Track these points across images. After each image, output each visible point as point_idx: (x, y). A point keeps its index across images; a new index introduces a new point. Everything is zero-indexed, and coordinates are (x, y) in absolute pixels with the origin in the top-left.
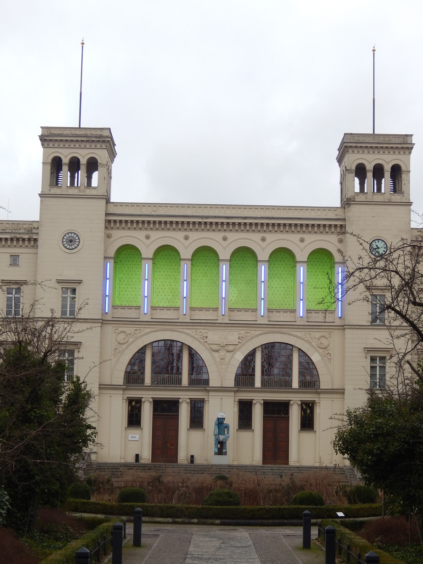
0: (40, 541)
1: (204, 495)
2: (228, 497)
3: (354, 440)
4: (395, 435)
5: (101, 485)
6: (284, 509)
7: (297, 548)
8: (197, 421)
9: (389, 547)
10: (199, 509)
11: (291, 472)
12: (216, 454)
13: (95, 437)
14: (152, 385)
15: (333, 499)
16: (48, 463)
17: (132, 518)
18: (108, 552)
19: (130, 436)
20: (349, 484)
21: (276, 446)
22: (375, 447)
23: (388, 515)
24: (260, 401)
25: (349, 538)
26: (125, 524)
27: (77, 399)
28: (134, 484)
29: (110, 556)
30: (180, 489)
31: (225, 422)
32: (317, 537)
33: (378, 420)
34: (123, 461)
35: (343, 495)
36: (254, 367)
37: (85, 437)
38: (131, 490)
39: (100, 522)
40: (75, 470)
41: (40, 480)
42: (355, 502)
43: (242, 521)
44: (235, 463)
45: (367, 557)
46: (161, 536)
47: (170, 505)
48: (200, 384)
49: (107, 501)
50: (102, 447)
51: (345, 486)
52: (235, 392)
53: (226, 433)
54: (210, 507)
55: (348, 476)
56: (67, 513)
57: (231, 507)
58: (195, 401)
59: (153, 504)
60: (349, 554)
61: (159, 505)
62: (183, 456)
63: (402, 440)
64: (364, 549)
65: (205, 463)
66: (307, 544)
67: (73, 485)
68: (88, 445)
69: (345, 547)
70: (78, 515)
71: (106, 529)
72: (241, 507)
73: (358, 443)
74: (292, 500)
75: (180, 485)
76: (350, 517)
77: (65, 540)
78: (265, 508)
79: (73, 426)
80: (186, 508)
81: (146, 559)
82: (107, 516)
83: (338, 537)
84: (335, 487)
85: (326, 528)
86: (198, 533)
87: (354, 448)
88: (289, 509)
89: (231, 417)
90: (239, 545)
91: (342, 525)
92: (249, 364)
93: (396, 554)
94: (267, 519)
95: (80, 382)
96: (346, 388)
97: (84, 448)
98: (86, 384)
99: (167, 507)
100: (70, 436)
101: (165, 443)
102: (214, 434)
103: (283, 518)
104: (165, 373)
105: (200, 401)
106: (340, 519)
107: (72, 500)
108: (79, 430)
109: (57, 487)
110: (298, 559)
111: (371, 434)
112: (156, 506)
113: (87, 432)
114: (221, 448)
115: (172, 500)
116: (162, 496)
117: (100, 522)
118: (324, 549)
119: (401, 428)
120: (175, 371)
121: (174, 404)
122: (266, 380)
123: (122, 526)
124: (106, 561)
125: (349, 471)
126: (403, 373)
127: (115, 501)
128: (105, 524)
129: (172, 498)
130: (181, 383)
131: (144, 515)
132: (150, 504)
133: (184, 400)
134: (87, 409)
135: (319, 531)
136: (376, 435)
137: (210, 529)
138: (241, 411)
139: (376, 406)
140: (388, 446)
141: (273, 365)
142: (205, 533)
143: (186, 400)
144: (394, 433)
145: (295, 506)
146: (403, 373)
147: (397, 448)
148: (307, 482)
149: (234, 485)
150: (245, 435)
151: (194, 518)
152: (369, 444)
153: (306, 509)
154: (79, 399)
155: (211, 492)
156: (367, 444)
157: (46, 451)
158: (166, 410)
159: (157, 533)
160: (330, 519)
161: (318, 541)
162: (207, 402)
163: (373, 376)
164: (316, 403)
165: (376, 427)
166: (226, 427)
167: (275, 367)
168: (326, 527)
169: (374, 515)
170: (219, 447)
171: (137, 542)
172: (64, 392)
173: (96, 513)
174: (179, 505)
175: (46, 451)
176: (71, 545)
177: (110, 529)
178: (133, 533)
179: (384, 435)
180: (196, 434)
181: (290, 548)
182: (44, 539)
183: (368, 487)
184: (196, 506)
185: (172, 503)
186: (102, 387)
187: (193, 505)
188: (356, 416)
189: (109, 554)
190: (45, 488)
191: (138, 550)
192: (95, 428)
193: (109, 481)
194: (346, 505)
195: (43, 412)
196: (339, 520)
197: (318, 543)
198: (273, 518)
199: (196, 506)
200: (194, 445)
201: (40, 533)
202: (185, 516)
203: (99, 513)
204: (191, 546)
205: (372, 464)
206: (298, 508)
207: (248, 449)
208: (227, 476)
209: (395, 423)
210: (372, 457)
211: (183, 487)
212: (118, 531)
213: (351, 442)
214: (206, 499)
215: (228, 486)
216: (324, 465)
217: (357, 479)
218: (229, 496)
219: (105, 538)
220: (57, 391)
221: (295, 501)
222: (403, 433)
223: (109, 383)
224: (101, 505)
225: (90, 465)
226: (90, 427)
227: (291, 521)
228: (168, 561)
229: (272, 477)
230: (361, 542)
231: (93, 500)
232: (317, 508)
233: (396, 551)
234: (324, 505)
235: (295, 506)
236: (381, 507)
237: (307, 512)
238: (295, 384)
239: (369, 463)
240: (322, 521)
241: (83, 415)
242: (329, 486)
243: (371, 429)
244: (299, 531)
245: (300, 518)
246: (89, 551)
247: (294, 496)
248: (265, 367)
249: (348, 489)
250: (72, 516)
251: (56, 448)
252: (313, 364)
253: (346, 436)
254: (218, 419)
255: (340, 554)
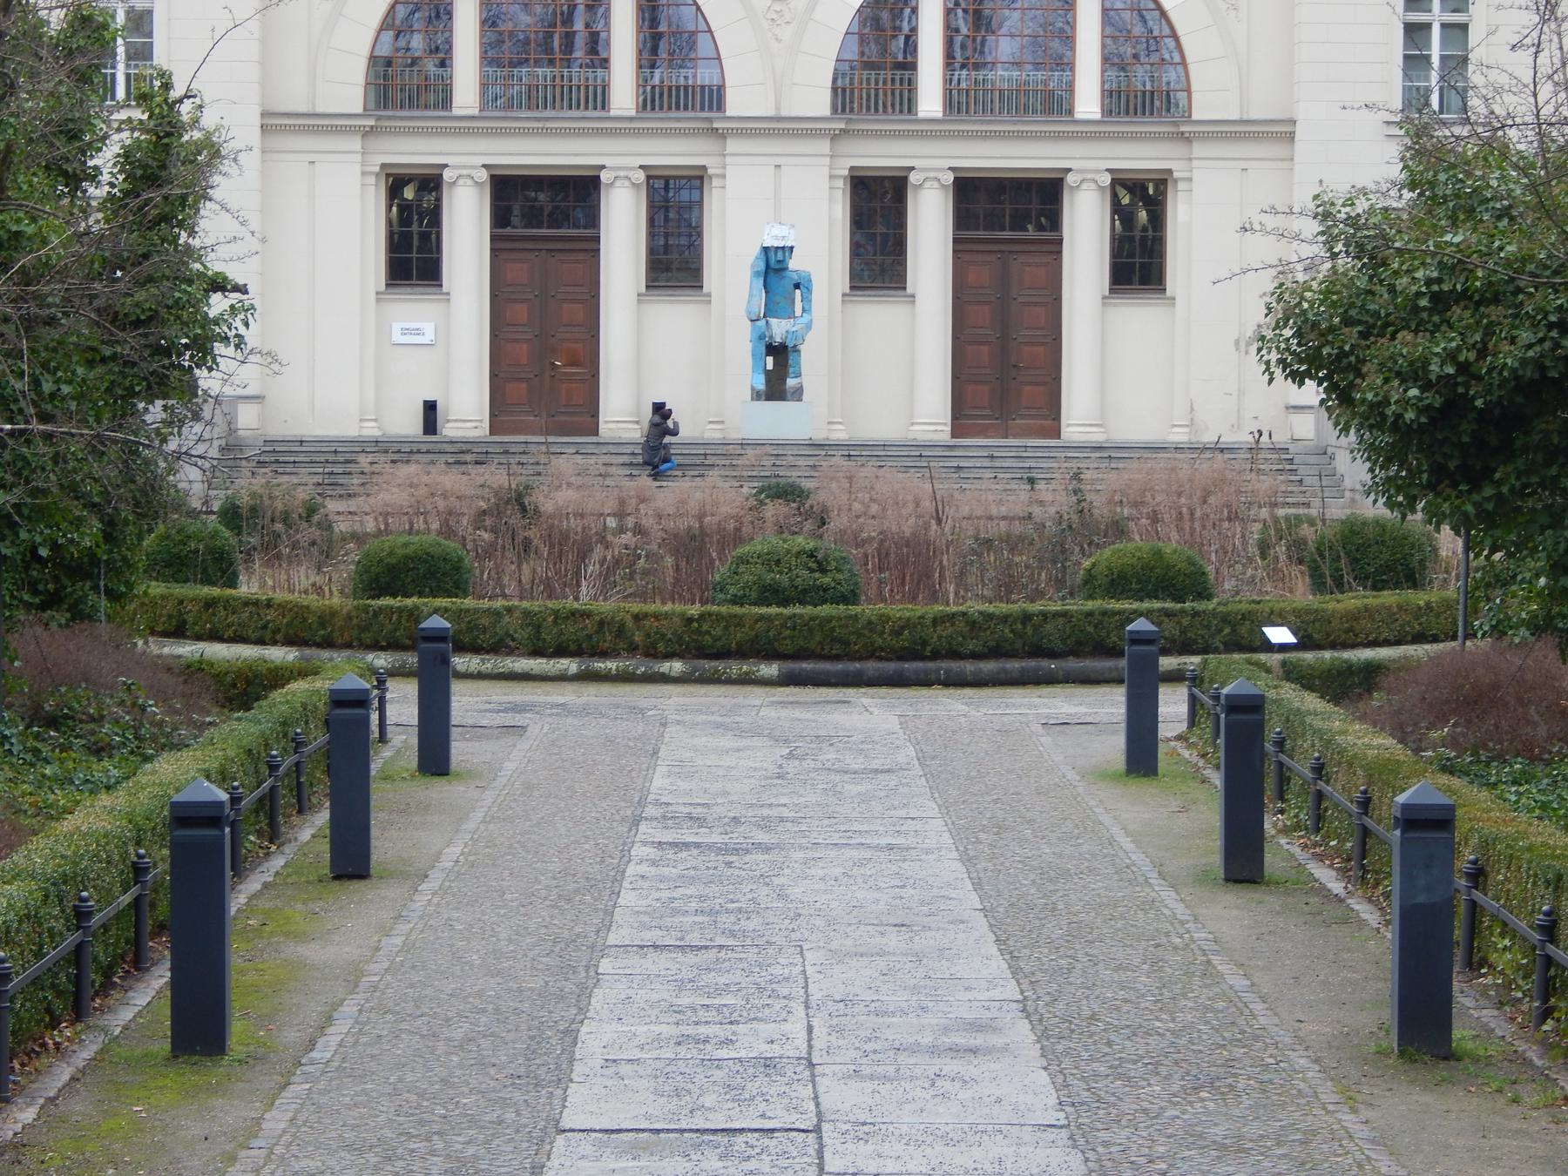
0: (29, 757)
1: (712, 561)
2: (812, 571)
3: (1348, 322)
4: (1521, 297)
5: (279, 526)
6: (1044, 615)
7: (1103, 776)
8: (675, 262)
9: (1488, 764)
10: (690, 620)
11: (1074, 464)
12: (757, 396)
13: (247, 325)
14: (485, 114)
15: (1250, 572)
16: (48, 437)
17: (412, 659)
18: (314, 800)
19: (397, 328)
20: (1314, 512)
21: (1006, 368)
22: (1438, 350)
23: (1483, 636)
24: (940, 175)
25: (1318, 732)
26: (381, 684)
27: (163, 167)
28: (419, 524)
29: (322, 817)
30: (610, 538)
31: (794, 264)
32: (1183, 727)
33: (1448, 238)
34: (371, 431)
35: (1290, 557)
36: (914, 30)
37: (203, 327)
38: (405, 545)
39: (278, 677)
40: (163, 465)
41: (15, 506)
42: (1340, 585)
43: (871, 667)
44: (840, 434)
45: (1405, 807)
46: (534, 729)
47: (570, 604)
48: (686, 108)
49: (306, 592)
50: (276, 367)
51: (1297, 517)
52: (835, 137)
53: (798, 312)
54: (736, 609)
55: (1308, 481)
56: (141, 643)
57: (825, 610)
58: (667, 179)
59: (499, 603)
60: (1320, 796)
61: (525, 604)
62: (620, 412)
63: (1553, 318)
64: (1385, 774)
65: (712, 434)
66: (1142, 756)
67: (161, 528)
68: (214, 360)
69: (1302, 767)
70: (187, 650)
71: (304, 706)
72: (866, 609)
73: (1364, 335)
74: (1079, 579)
75: (612, 523)
76: (1319, 647)
77: (132, 752)
78: (964, 614)
79: (150, 280)
80: (637, 618)
81: (471, 826)
82: (307, 651)
83: (1274, 728)
84: (1257, 527)
85: (1225, 691)
86: (688, 717)
87: (1347, 355)
88: (1064, 614)
89: (821, 240)
90: (856, 763)
91: (1288, 680)
92: (894, 21)
93: (1518, 793)
94: (975, 656)
95: (175, 94)
96: (1300, 116)
97: (201, 373)
98: (198, 101)
99: (556, 613)
100: (138, 323)
101: (545, 360)
102: (749, 313)
103: (1038, 651)
104: (537, 63)
105: (690, 178)
106: (1279, 657)
107: (157, 588)
108: (177, 295)
109: (90, 534)
110: (1107, 819)
111: (1419, 294)
112: (509, 610)
113: (208, 305)
114: (779, 369)
115: (578, 585)
116: (534, 571)
117: (278, 677)
118: (1217, 778)
119: (1546, 267)
120: (579, 53)
121: (576, 195)
122: (963, 85)
123: (366, 691)
124: (305, 835)
125: (1312, 459)
126: (1559, 34)
127: (342, 592)
128: (298, 686)
129: (577, 574)
130: (605, 105)
131: (461, 648)
132: (485, 604)
133: (622, 174)
134: (207, 209)
135: (1193, 701)
136: (1441, 302)
137: (740, 700)
138: (861, 220)
139: (1442, 177)
140: (1490, 346)
141: (994, 25)
142: (719, 719)
143: (630, 174)
144: (1519, 290)
145: (1091, 605)
146: (1559, 34)
147: (1531, 353)
148: (1135, 505)
149: (837, 523)
150: (878, 313)
151: (669, 656)
152: (1409, 337)
153: (1138, 614)
154: (169, 172)
155: (740, 551)
156: (1399, 335)
157: (36, 383)
158: (545, 214)
159: (518, 719)
160: (1236, 656)
161: (1190, 746)
162: (715, 182)
163: (1415, 62)
164: (1176, 181)
165: (1441, 265)
166: (797, 286)
167: (1004, 30)
168: (1223, 686)
169: (1419, 638)
170: (770, 366)
171: (434, 758)
172: (106, 137)
173: (261, 642)
174: (606, 607)
175: (36, 383)
176: (154, 772)
177: (321, 705)
178: (416, 722)
179: (1477, 297)
180: (674, 315)
181: (1071, 775)
182: (45, 750)
183: (1404, 517)
184: (679, 608)
185: (577, 599)
186: (275, 124)
187: (664, 603)
188: (1352, 221)
189: (313, 809)
190: (38, 539)
191: (437, 789)
192: (242, 289)
193: (311, 510)
194: (1302, 595)
195: (18, 221)
196: (1275, 659)
197: (1186, 754)
198: (996, 652)
199: (679, 608)
200: (660, 356)
201: (28, 727)
202: (633, 649)
203: (274, 643)
204: (662, 769)
205: (1423, 420)
206: (1104, 613)
207: (888, 372)
208: (807, 484)
209: (1520, 249)
210: (1423, 389)
211: (621, 530)
212: (350, 715)
213: (1332, 329)
214: (717, 577)
215: (808, 526)
216: (1209, 438)
217: (1351, 486)
218: (814, 566)
219: (298, 744)
220: (74, 134)
221: (1091, 585)
222: (1556, 291)
223: (303, 109)
224: (283, 607)
225: (232, 447)
226: (219, 285)
227: (1072, 664)
228: (563, 830)
229: (997, 491)
230: (1370, 747)
231: (248, 587)
232: (1183, 611)
233: (1515, 782)
234: (1209, 597)
235: (1091, 605)
236: (1448, 605)
237: (1141, 625)
238: (1088, 102)
239: (1410, 415)
240: (1205, 662)
241: (192, 233)
242: (1229, 519)
243: (1419, 274)
244: (1110, 704)
245: (1118, 653)
246: (224, 796)
247: (1087, 563)
248: (957, 30)
249: (1306, 531)
250: (160, 656)
251: (80, 371)
252: (1163, 14)
253: (1312, 303)
254: (766, 250)
255: (1281, 797)
